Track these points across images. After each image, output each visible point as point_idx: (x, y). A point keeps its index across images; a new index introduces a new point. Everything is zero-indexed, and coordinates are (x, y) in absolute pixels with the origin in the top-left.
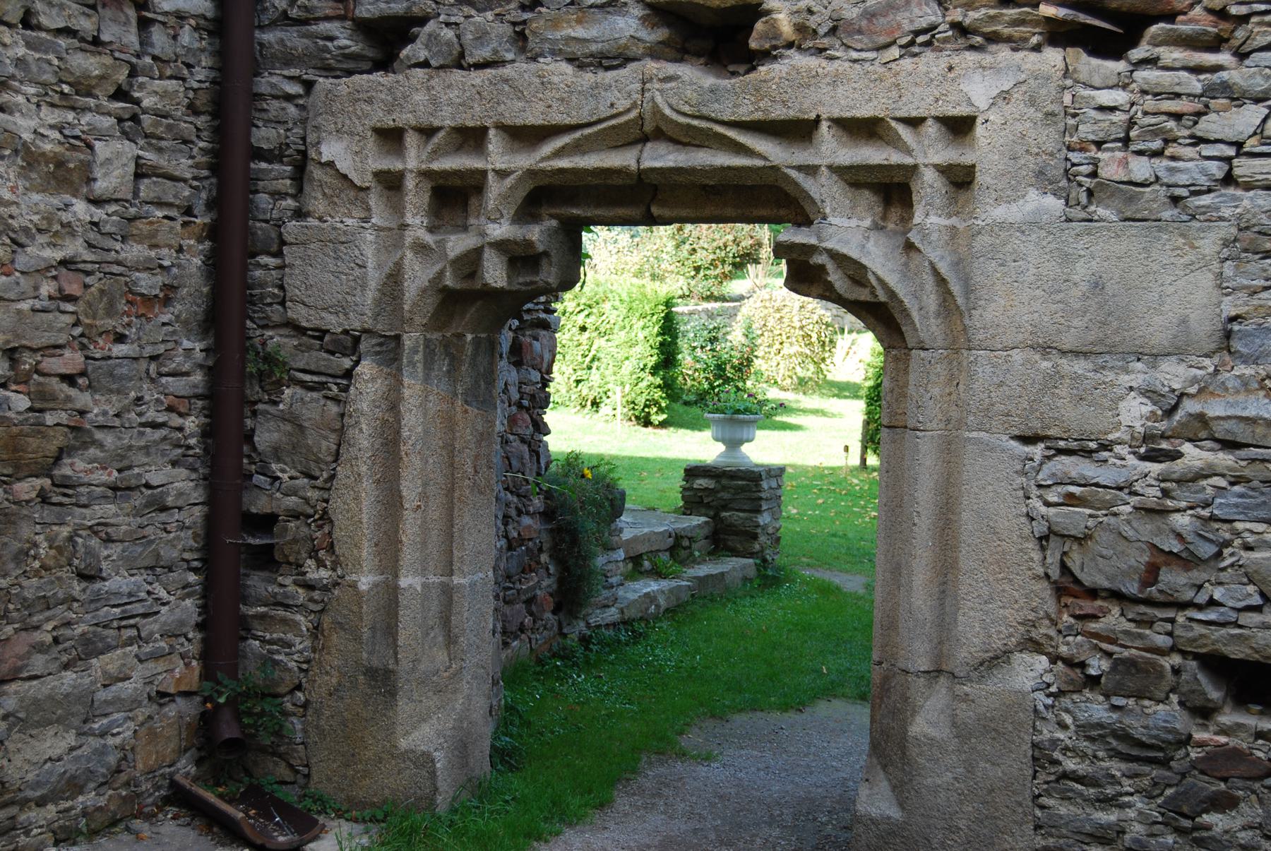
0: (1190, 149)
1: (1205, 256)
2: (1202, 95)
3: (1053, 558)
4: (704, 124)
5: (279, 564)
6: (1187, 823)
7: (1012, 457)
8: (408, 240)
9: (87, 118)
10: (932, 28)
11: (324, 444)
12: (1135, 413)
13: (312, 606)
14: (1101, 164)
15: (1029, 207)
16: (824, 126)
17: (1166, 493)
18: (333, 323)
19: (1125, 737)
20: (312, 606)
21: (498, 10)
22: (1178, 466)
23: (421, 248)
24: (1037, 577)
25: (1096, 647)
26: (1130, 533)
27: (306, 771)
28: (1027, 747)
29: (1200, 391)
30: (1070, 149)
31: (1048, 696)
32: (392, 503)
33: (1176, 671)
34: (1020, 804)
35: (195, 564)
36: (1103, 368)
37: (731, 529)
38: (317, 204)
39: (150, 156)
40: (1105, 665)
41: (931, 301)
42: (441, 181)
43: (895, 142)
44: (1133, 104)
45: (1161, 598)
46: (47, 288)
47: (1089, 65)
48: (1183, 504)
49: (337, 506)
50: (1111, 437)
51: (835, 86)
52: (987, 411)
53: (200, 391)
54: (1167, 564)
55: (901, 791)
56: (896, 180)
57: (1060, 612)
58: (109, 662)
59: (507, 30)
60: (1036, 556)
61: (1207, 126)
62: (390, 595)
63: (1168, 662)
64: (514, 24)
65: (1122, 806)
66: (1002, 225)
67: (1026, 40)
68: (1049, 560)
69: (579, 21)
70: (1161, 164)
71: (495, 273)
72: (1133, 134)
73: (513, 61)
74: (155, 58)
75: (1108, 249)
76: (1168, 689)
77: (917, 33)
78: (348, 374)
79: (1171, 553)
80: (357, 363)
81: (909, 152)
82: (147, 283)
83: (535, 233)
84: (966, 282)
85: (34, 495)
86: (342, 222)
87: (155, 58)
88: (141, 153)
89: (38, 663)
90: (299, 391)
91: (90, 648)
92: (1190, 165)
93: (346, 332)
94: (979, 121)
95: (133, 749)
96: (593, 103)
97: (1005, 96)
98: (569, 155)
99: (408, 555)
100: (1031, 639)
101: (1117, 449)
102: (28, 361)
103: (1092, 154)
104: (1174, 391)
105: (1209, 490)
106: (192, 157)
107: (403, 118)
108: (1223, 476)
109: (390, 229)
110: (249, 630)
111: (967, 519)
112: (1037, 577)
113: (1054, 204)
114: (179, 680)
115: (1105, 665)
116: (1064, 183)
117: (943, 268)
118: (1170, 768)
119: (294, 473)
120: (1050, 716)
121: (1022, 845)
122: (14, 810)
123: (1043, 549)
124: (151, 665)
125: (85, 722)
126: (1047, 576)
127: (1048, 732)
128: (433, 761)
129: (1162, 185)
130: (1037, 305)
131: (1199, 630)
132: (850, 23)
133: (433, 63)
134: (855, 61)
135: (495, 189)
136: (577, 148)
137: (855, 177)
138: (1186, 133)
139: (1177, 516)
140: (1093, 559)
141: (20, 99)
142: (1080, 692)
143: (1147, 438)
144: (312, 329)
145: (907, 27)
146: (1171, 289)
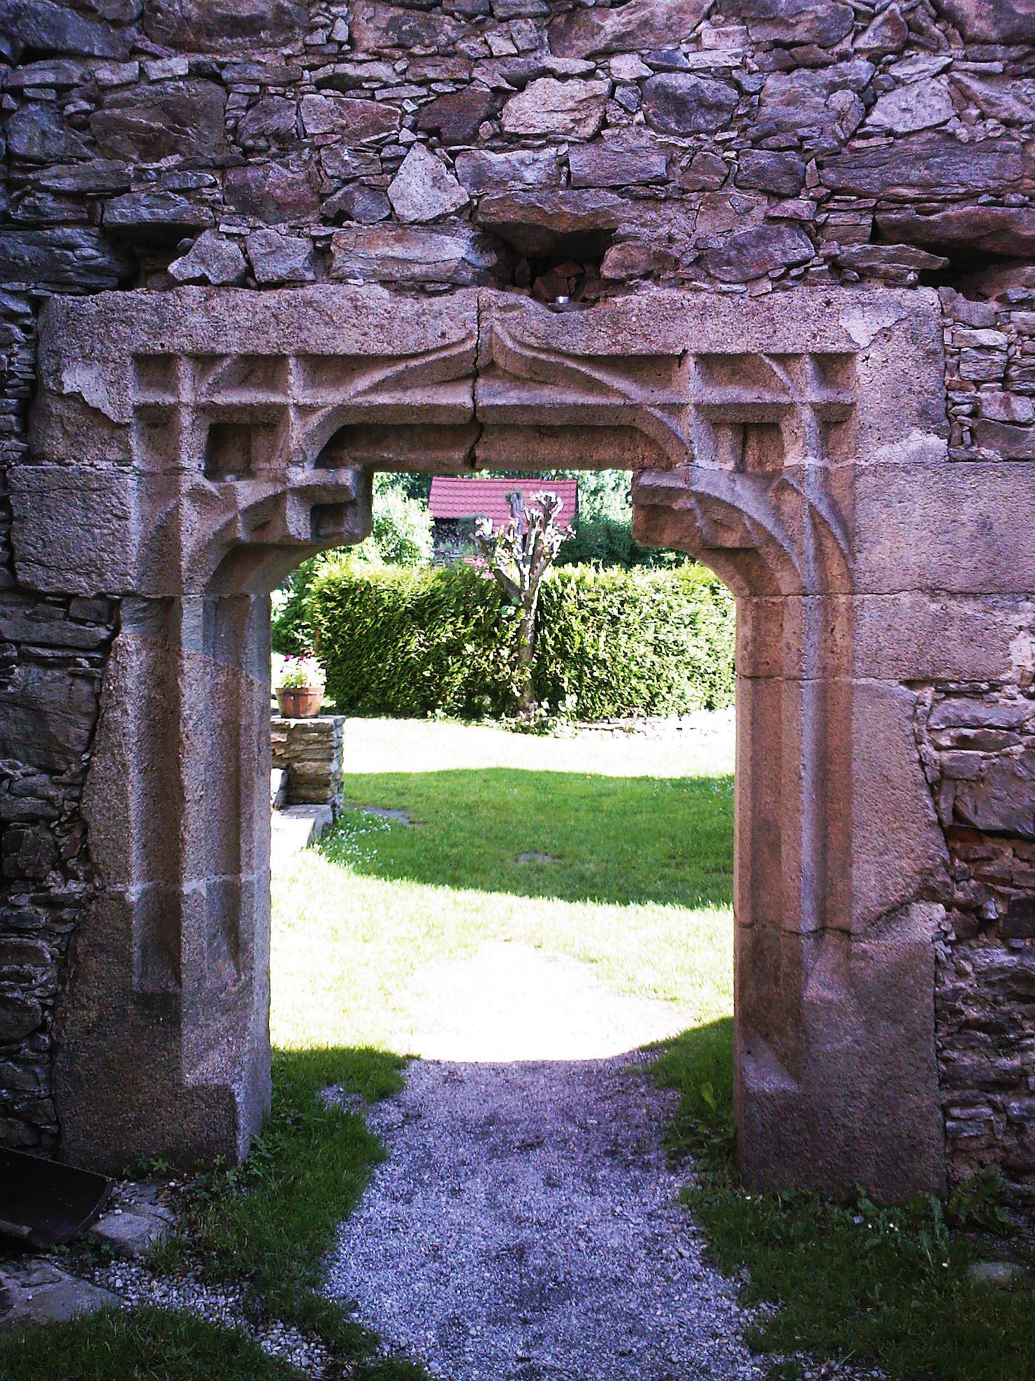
4: (553, 359)
5: (11, 881)
7: (904, 703)
8: (185, 487)
11: (74, 731)
15: (914, 447)
16: (691, 362)
18: (82, 584)
21: (293, 223)
23: (198, 495)
27: (54, 1129)
28: (929, 1000)
34: (924, 1060)
36: (994, 608)
42: (224, 418)
44: (1010, 344)
49: (95, 804)
50: (1003, 677)
52: (875, 656)
55: (793, 1063)
57: (952, 859)
62: (166, 907)
64: (315, 239)
66: (887, 466)
67: (903, 276)
68: (943, 806)
69: (399, 239)
73: (313, 282)
77: (790, 266)
78: (106, 647)
80: (116, 632)
81: (785, 390)
86: (91, 465)
93: (101, 596)
94: (860, 357)
96: (420, 332)
97: (886, 333)
98: (389, 391)
109: (152, 474)
112: (930, 824)
113: (936, 443)
116: (945, 423)
121: (927, 1102)
123: (933, 794)
128: (232, 1096)
132: (717, 252)
134: (724, 293)
135: (297, 432)
137: (715, 417)
144: (52, 594)
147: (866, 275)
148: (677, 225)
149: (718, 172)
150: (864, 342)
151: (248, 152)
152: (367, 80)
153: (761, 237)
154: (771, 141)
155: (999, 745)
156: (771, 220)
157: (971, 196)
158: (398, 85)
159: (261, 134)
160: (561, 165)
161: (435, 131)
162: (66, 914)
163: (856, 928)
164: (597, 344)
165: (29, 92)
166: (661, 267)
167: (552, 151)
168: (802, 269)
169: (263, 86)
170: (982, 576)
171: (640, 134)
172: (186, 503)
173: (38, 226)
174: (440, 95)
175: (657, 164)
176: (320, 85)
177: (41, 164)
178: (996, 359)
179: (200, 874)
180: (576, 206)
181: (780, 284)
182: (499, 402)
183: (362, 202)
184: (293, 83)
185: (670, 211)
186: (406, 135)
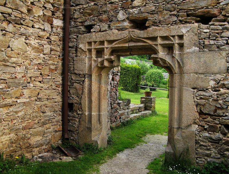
0: (220, 39)
1: (223, 56)
2: (222, 30)
3: (198, 109)
4: (139, 38)
6: (222, 153)
7: (191, 91)
8: (92, 59)
9: (42, 42)
10: (176, 21)
12: (212, 83)
13: (79, 117)
14: (205, 42)
15: (193, 49)
16: (158, 37)
17: (218, 97)
18: (81, 73)
19: (211, 138)
20: (79, 117)
22: (219, 92)
24: (196, 112)
25: (206, 124)
26: (212, 104)
28: (194, 140)
29: (223, 80)
30: (200, 39)
31: (198, 132)
32: (90, 101)
33: (220, 127)
35: (61, 111)
36: (206, 76)
37: (148, 106)
38: (79, 54)
39: (53, 47)
40: (208, 126)
41: (177, 65)
42: (97, 50)
43: (170, 40)
44: (210, 32)
45: (217, 115)
46: (36, 67)
47: (202, 26)
48: (221, 99)
50: (208, 88)
51: (160, 31)
53: (61, 84)
54: (218, 109)
56: (171, 46)
57: (200, 118)
58: (47, 126)
59: (107, 25)
60: (196, 108)
61: (223, 35)
62: (90, 116)
63: (219, 126)
64: (108, 24)
65: (211, 150)
66: (188, 53)
67: (192, 22)
68: (198, 109)
69: (119, 23)
70: (215, 42)
71: (106, 64)
72: (210, 36)
74: (54, 33)
75: (207, 56)
76: (218, 130)
77: (173, 22)
78: (84, 81)
79: (219, 107)
80: (85, 79)
81: (172, 41)
82: (52, 67)
83: (112, 57)
84: (183, 62)
85: (34, 100)
87: (54, 33)
88: (51, 47)
89: (36, 126)
90: (76, 84)
91: (44, 124)
92: (220, 41)
93: (83, 74)
94: (184, 35)
95: (51, 139)
97: (188, 31)
98: (117, 45)
99: (93, 109)
100: (195, 122)
101: (209, 90)
102: (33, 79)
103: (203, 40)
104: (219, 80)
105: (225, 97)
106: (60, 48)
107: (92, 40)
108: (228, 94)
110: (69, 121)
111: (184, 102)
114: (58, 129)
115: (208, 126)
116: (199, 45)
117: (179, 60)
118: (219, 144)
119: (76, 97)
120: (198, 135)
122: (32, 148)
123: (197, 107)
124: (54, 126)
125: (43, 135)
126: (197, 112)
127: (198, 138)
129: (215, 45)
130: (195, 66)
131: (224, 120)
132: (162, 21)
133: (96, 31)
134: (163, 27)
136: (119, 43)
137: (163, 46)
138: (219, 36)
139: (220, 101)
140: (205, 108)
141: (32, 38)
142: (203, 131)
143: (214, 88)
145: (172, 21)
146: (218, 62)
147: (186, 22)
148: (157, 17)
149: (162, 9)
150: (185, 33)
151: (101, 14)
152: (115, 2)
153: (169, 18)
154: (170, 3)
155: (207, 99)
156: (170, 15)
157: (202, 8)
158: (119, 2)
159: (102, 11)
160: (140, 10)
161: (123, 8)
162: (79, 116)
163: (183, 128)
164: (145, 36)
165: (76, 10)
166: (155, 24)
167: (139, 8)
168: (175, 22)
169: (102, 5)
170: (204, 71)
171: (151, 4)
172: (93, 61)
173: (77, 27)
174: (124, 2)
175: (153, 8)
176: (109, 3)
177: (77, 19)
178: (207, 34)
179: (94, 112)
180: (142, 16)
181: (171, 25)
182: (131, 45)
183: (114, 19)
184: (106, 4)
185: (155, 15)
186: (120, 9)
